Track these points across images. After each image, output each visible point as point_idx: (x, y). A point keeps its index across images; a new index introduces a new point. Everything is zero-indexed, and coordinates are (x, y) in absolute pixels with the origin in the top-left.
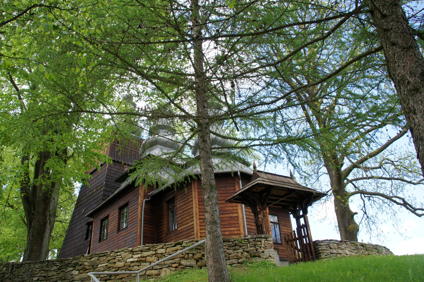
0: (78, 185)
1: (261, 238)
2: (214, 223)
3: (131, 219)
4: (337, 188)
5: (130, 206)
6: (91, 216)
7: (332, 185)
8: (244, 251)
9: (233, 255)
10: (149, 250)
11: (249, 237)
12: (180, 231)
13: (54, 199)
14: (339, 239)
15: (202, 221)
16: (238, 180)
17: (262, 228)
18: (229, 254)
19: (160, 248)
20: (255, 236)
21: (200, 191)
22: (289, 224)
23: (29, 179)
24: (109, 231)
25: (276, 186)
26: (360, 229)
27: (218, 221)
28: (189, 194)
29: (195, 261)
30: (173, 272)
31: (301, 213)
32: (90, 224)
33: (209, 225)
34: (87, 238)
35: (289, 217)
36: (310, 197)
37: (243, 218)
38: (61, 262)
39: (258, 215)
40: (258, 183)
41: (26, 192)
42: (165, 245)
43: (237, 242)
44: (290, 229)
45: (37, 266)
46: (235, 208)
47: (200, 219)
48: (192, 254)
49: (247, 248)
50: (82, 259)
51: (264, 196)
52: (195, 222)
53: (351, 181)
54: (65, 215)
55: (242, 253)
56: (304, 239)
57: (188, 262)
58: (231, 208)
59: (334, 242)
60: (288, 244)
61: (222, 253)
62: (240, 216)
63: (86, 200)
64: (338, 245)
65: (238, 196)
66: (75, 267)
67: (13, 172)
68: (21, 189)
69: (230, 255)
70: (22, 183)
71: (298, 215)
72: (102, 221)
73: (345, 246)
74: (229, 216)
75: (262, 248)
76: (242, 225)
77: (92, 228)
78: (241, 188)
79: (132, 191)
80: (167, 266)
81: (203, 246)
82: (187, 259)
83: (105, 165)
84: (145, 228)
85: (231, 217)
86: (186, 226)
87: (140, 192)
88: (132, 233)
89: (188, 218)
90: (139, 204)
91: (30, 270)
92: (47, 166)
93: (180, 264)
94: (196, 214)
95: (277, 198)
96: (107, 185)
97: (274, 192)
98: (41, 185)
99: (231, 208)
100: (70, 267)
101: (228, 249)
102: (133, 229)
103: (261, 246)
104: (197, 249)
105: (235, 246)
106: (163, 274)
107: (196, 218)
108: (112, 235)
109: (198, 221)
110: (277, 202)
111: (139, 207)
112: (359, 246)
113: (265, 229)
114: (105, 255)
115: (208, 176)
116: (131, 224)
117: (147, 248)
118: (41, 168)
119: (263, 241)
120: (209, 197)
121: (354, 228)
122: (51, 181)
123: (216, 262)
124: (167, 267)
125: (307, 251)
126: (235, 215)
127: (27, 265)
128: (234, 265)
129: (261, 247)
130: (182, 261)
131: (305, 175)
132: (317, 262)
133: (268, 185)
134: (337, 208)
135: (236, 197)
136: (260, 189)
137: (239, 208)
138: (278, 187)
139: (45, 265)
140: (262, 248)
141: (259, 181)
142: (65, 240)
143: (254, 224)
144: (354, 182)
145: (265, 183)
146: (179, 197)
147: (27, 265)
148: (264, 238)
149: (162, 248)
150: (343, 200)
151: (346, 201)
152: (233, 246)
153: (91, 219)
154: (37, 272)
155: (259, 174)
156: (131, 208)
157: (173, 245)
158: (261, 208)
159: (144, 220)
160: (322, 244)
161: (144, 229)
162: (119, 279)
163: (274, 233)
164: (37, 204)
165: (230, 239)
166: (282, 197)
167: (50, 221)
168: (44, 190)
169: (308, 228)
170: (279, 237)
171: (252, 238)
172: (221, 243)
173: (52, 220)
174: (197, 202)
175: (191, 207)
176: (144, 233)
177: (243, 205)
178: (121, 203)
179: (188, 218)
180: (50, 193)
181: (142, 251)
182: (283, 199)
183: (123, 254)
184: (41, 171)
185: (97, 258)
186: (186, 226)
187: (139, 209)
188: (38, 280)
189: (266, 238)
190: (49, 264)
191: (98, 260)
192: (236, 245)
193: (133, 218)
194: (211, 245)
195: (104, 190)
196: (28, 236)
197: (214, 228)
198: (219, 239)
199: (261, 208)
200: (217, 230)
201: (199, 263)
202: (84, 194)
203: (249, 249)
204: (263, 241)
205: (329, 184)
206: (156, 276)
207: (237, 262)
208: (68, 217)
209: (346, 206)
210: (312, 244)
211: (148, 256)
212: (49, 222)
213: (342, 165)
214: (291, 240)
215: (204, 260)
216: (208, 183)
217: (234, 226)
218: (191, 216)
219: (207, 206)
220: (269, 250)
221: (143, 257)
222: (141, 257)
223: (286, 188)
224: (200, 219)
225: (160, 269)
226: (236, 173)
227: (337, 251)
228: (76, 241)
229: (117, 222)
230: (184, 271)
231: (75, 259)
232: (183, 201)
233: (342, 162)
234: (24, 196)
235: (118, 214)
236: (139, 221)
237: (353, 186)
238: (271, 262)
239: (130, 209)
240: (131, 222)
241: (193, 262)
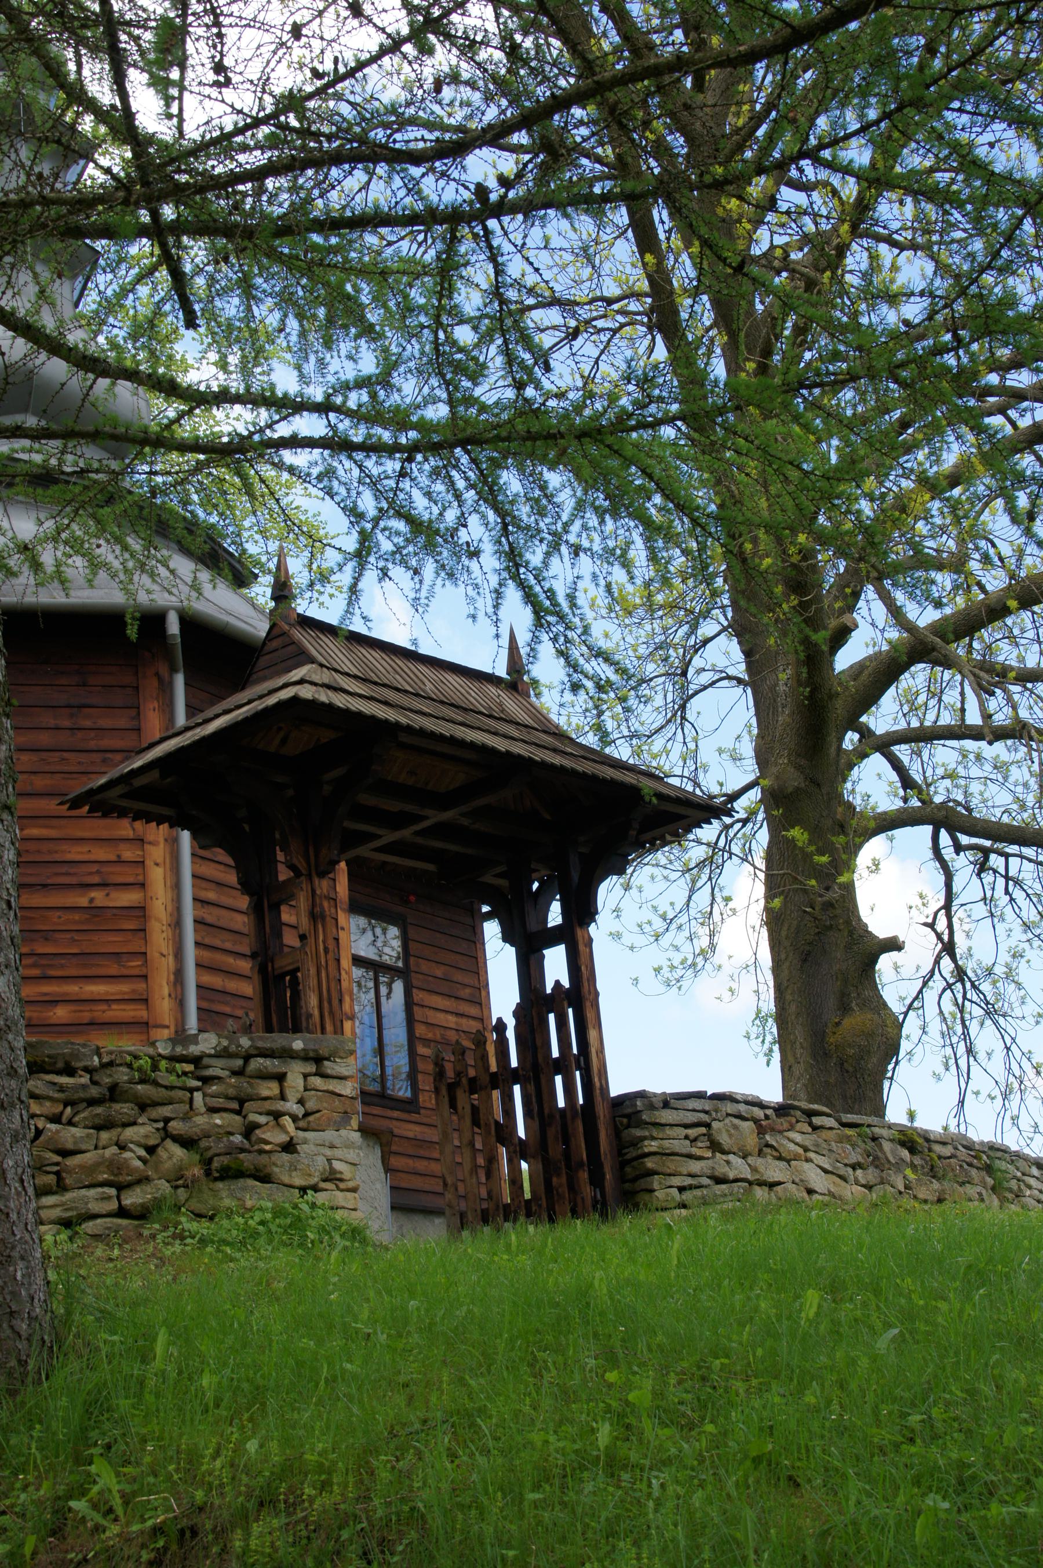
4: (794, 780)
7: (762, 758)
8: (166, 1134)
9: (89, 1158)
11: (208, 1043)
14: (772, 1091)
16: (164, 671)
17: (296, 996)
18: (65, 1153)
20: (245, 1042)
25: (408, 729)
26: (905, 1046)
31: (555, 915)
35: (477, 940)
36: (626, 816)
37: (177, 924)
39: (276, 908)
40: (295, 699)
43: (122, 1075)
44: (474, 1011)
46: (128, 854)
49: (186, 1118)
53: (884, 745)
55: (151, 1150)
56: (558, 1079)
58: (101, 853)
59: (742, 1108)
60: (453, 1105)
64: (761, 1131)
65: (155, 774)
69: (72, 1161)
71: (533, 926)
73: (808, 1140)
74: (83, 902)
85: (93, 910)
95: (409, 808)
99: (101, 853)
101: (56, 1119)
103: (280, 1106)
105: (108, 1099)
112: (887, 1146)
113: (313, 1001)
121: (871, 1035)
125: (567, 1155)
126: (128, 898)
128: (89, 1227)
129: (277, 1115)
131: (607, 672)
132: (626, 1224)
133: (359, 715)
134: (777, 903)
135: (138, 782)
137: (157, 853)
138: (422, 732)
140: (287, 1121)
141: (301, 684)
143: (245, 966)
144: (902, 751)
145: (340, 701)
150: (824, 859)
151: (844, 861)
152: (92, 1102)
155: (304, 638)
158: (301, 865)
160: (667, 1116)
163: (373, 1025)
165: (76, 1056)
166: (443, 801)
169: (589, 1015)
170: (398, 1060)
171: (223, 1054)
177: (186, 836)
189: (318, 1060)
192: (114, 1094)
199: (301, 865)
203: (201, 1121)
204: (296, 1074)
205: (747, 749)
207: (114, 1205)
209: (835, 894)
210: (602, 1110)
213: (841, 635)
214: (472, 1081)
217: (114, 970)
220: (329, 1135)
223: (472, 746)
227: (754, 1170)
233: (845, 619)
237: (894, 776)
238: (339, 1215)
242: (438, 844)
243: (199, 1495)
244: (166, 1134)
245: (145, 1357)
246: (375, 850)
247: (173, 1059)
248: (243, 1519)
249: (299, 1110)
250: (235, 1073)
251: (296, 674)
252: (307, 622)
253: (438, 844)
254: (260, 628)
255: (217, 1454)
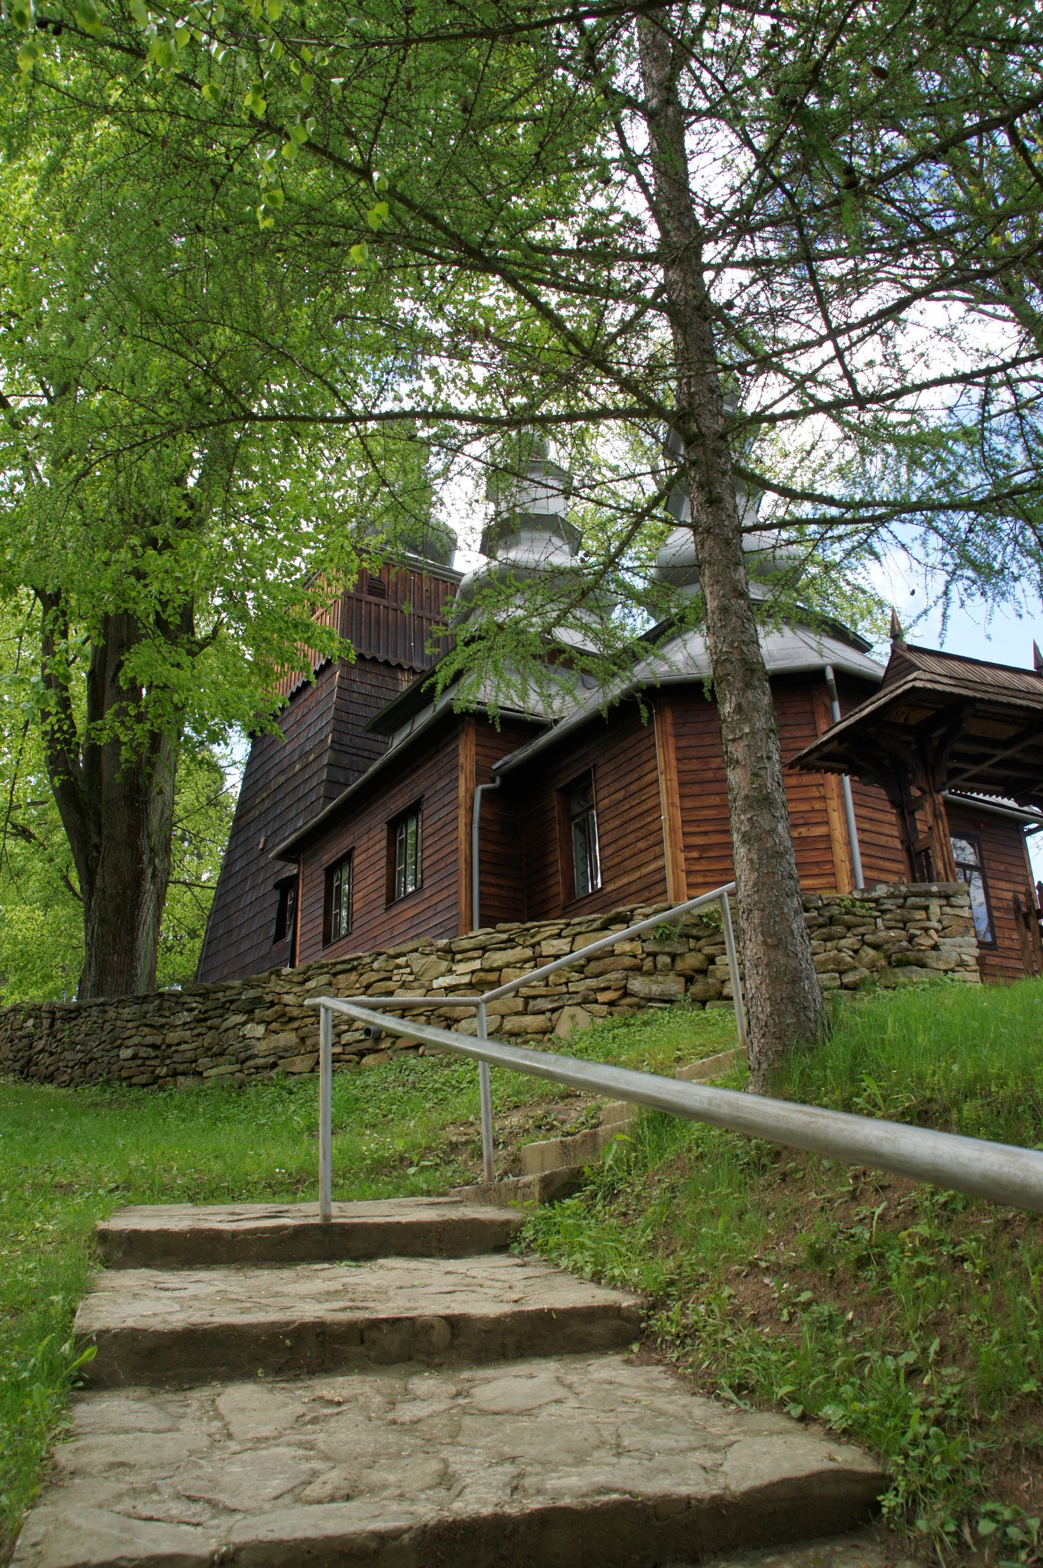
0: (235, 750)
1: (929, 895)
2: (762, 801)
3: (434, 858)
5: (426, 813)
6: (290, 855)
8: (864, 943)
10: (510, 943)
11: (881, 890)
12: (614, 896)
13: (161, 792)
15: (695, 854)
16: (827, 701)
17: (929, 863)
19: (552, 937)
20: (903, 889)
21: (683, 743)
22: (1020, 871)
23: (72, 725)
24: (356, 907)
25: (981, 700)
27: (779, 797)
28: (644, 758)
29: (682, 980)
30: (599, 1021)
32: (287, 886)
33: (744, 812)
34: (280, 935)
37: (849, 843)
38: (205, 995)
39: (912, 813)
40: (913, 688)
41: (68, 772)
42: (568, 925)
43: (835, 910)
45: (126, 1012)
46: (818, 806)
47: (688, 848)
48: (668, 954)
49: (874, 933)
50: (275, 985)
51: (935, 742)
52: (668, 860)
54: (199, 868)
55: (856, 952)
57: (657, 982)
60: (1028, 926)
61: (796, 913)
62: (838, 834)
63: (267, 804)
65: (835, 744)
66: (251, 1012)
67: (22, 681)
68: (51, 761)
70: (50, 738)
72: (330, 871)
75: (932, 932)
76: (844, 868)
77: (296, 899)
78: (838, 718)
79: (431, 758)
80: (578, 999)
81: (707, 926)
82: (649, 974)
83: (328, 674)
84: (485, 889)
86: (637, 874)
87: (462, 759)
88: (440, 907)
89: (641, 845)
90: (462, 790)
91: (108, 1027)
92: (130, 675)
93: (626, 993)
94: (672, 830)
96: (338, 746)
97: (974, 726)
98: (116, 742)
99: (803, 807)
100: (236, 1012)
102: (445, 894)
103: (928, 924)
104: (688, 937)
106: (563, 1029)
107: (673, 845)
108: (368, 917)
109: (681, 856)
110: (984, 767)
111: (462, 812)
113: (940, 865)
114: (354, 969)
115: (734, 630)
116: (436, 877)
117: (504, 936)
118: (108, 683)
119: (935, 905)
120: (739, 709)
122: (148, 726)
123: (775, 947)
124: (579, 1004)
126: (820, 831)
127: (94, 1012)
129: (926, 930)
130: (631, 981)
133: (951, 694)
135: (826, 749)
136: (916, 717)
139: (151, 1007)
140: (932, 932)
141: (917, 680)
142: (208, 944)
146: (605, 769)
147: (94, 1012)
148: (939, 895)
149: (559, 936)
152: (820, 926)
153: (292, 869)
154: (128, 1033)
155: (913, 657)
156: (431, 817)
157: (597, 924)
158: (925, 786)
159: (481, 862)
161: (481, 893)
162: (408, 1048)
164: (108, 807)
166: (1006, 745)
167: (155, 869)
168: (127, 761)
171: (891, 896)
172: (791, 877)
173: (160, 867)
174: (675, 784)
175: (650, 804)
176: (481, 906)
178: (397, 802)
179: (641, 845)
180: (148, 769)
181: (484, 949)
182: (1009, 753)
183: (418, 962)
184: (109, 693)
185: (324, 979)
186: (637, 874)
187: (462, 821)
188: (135, 1057)
189: (947, 897)
190: (167, 1004)
191: (330, 984)
192: (832, 921)
193: (440, 855)
194: (755, 885)
195: (329, 765)
196: (86, 921)
197: (765, 821)
198: (784, 863)
199: (925, 786)
200: (774, 830)
201: (696, 989)
202: (261, 784)
203: (883, 934)
204: (935, 905)
206: (539, 1037)
208: (209, 875)
211: (508, 965)
212: (150, 871)
215: (714, 976)
216: (735, 657)
217: (816, 871)
218: (652, 840)
219: (734, 740)
220: (958, 940)
221: (491, 970)
222: (482, 970)
223: (1021, 707)
224: (688, 848)
225: (553, 1010)
226: (820, 672)
228: (245, 946)
229: (384, 871)
230: (642, 1016)
231: (248, 985)
232: (624, 782)
234: (63, 784)
235: (384, 843)
236: (462, 865)
239: (427, 823)
240: (433, 870)
241: (674, 985)
242: (1005, 772)
243: (928, 1093)
244: (864, 943)
245: (883, 1028)
246: (967, 780)
247: (863, 900)
248: (956, 1103)
249: (939, 926)
250: (899, 907)
251: (910, 677)
252: (912, 649)
253: (1005, 772)
254: (881, 673)
255: (934, 1074)
